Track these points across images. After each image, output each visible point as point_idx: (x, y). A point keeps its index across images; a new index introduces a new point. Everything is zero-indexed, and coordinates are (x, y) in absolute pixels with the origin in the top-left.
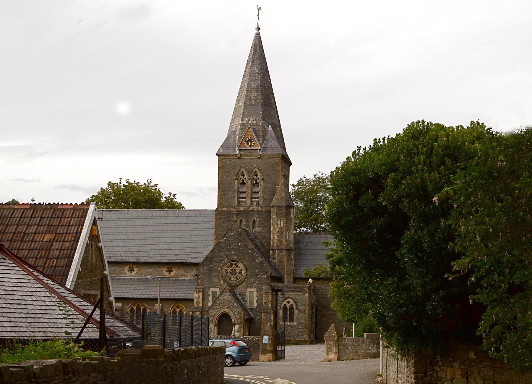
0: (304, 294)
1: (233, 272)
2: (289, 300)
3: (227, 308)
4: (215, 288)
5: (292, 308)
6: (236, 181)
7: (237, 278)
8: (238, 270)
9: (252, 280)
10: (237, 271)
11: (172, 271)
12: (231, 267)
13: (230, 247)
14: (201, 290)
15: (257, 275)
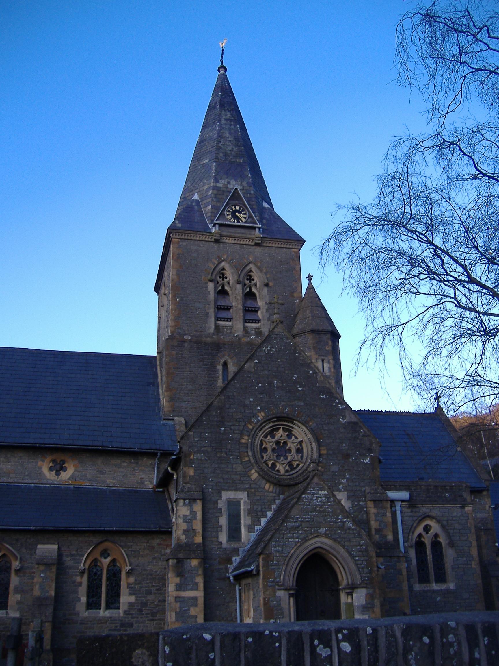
0: (463, 507)
1: (281, 449)
2: (428, 522)
3: (326, 535)
4: (236, 490)
5: (436, 544)
6: (211, 285)
7: (290, 464)
8: (292, 445)
9: (335, 468)
10: (289, 445)
11: (65, 469)
12: (273, 437)
13: (271, 384)
14: (196, 495)
15: (347, 456)
